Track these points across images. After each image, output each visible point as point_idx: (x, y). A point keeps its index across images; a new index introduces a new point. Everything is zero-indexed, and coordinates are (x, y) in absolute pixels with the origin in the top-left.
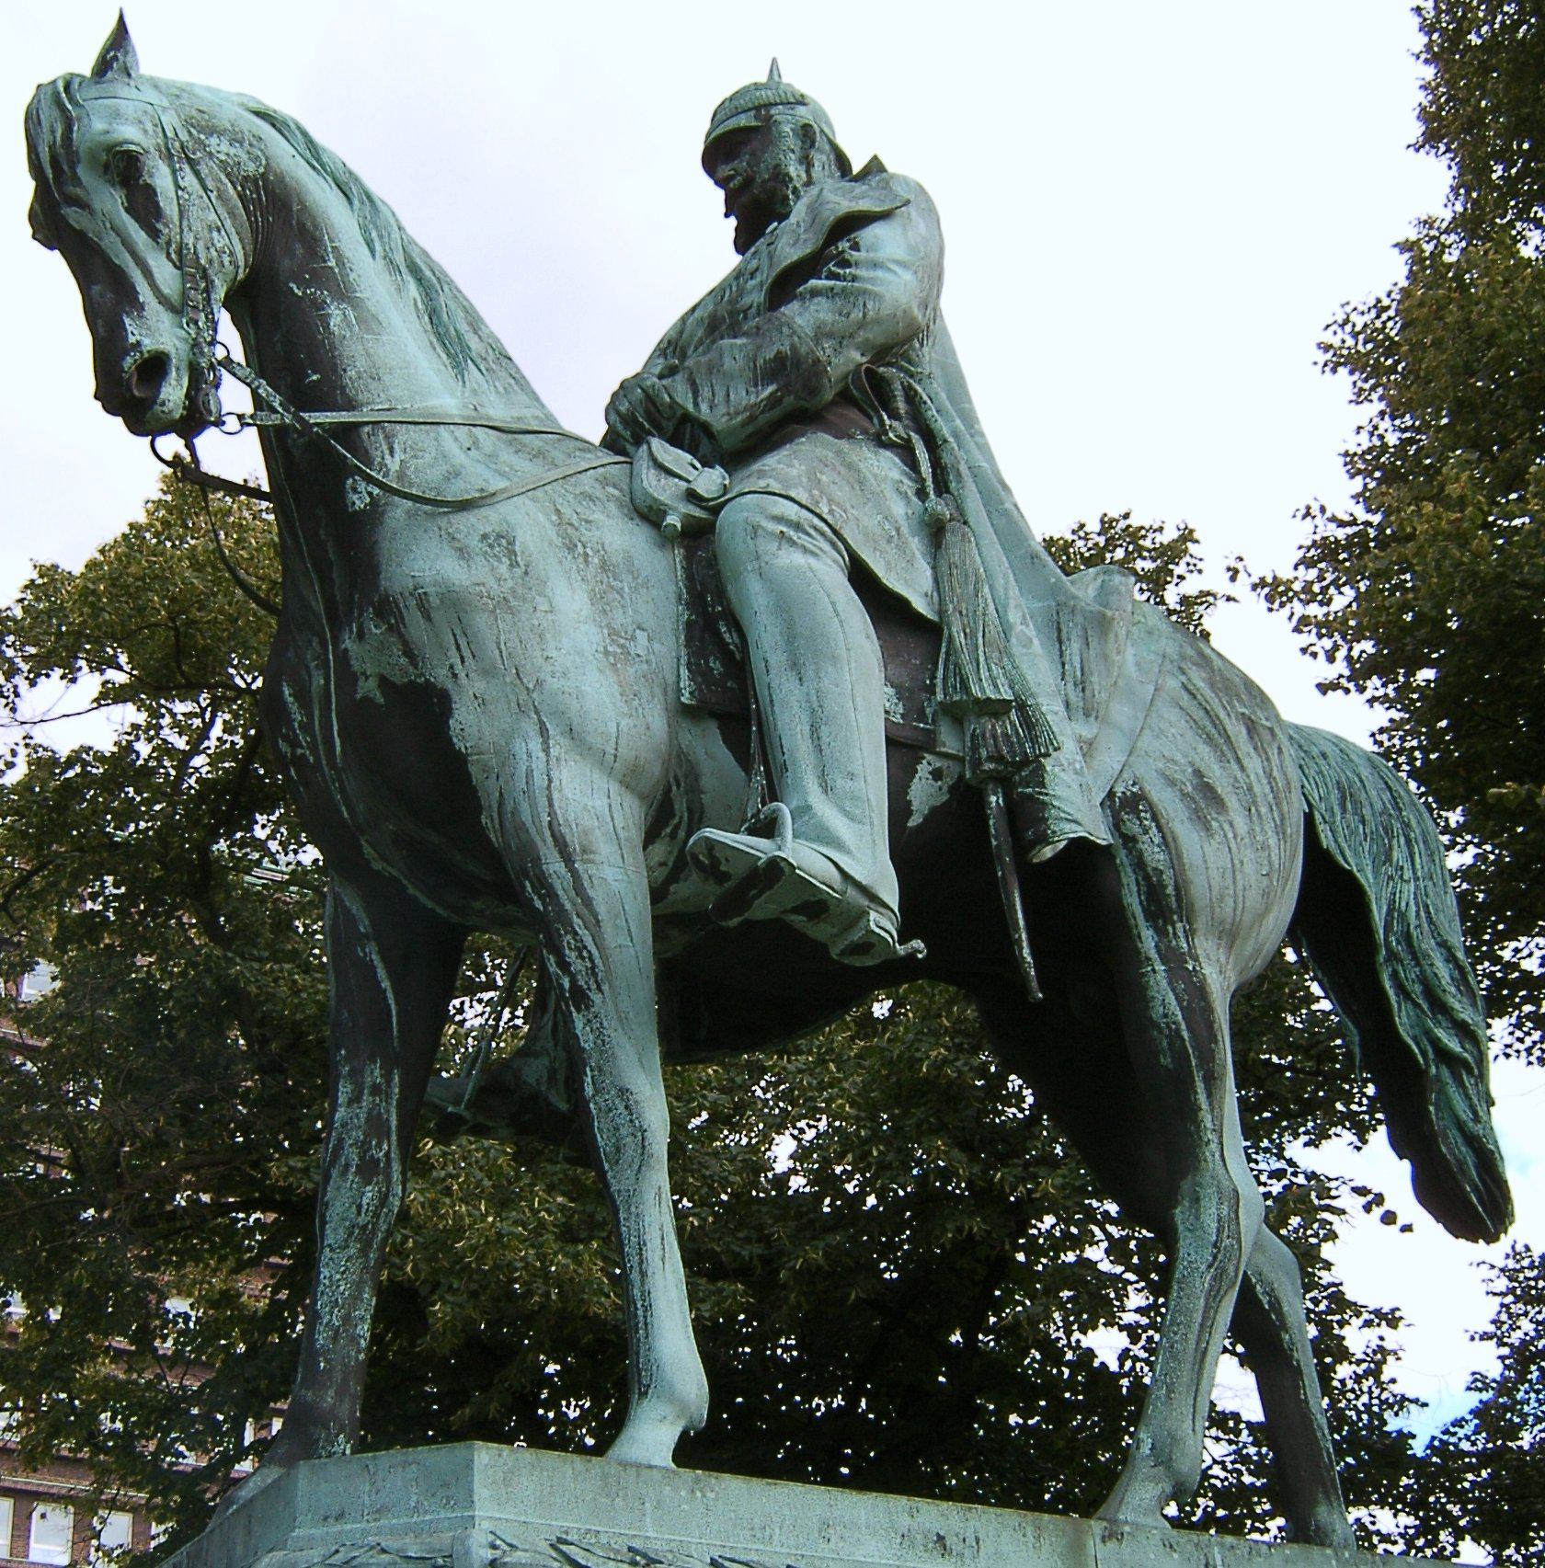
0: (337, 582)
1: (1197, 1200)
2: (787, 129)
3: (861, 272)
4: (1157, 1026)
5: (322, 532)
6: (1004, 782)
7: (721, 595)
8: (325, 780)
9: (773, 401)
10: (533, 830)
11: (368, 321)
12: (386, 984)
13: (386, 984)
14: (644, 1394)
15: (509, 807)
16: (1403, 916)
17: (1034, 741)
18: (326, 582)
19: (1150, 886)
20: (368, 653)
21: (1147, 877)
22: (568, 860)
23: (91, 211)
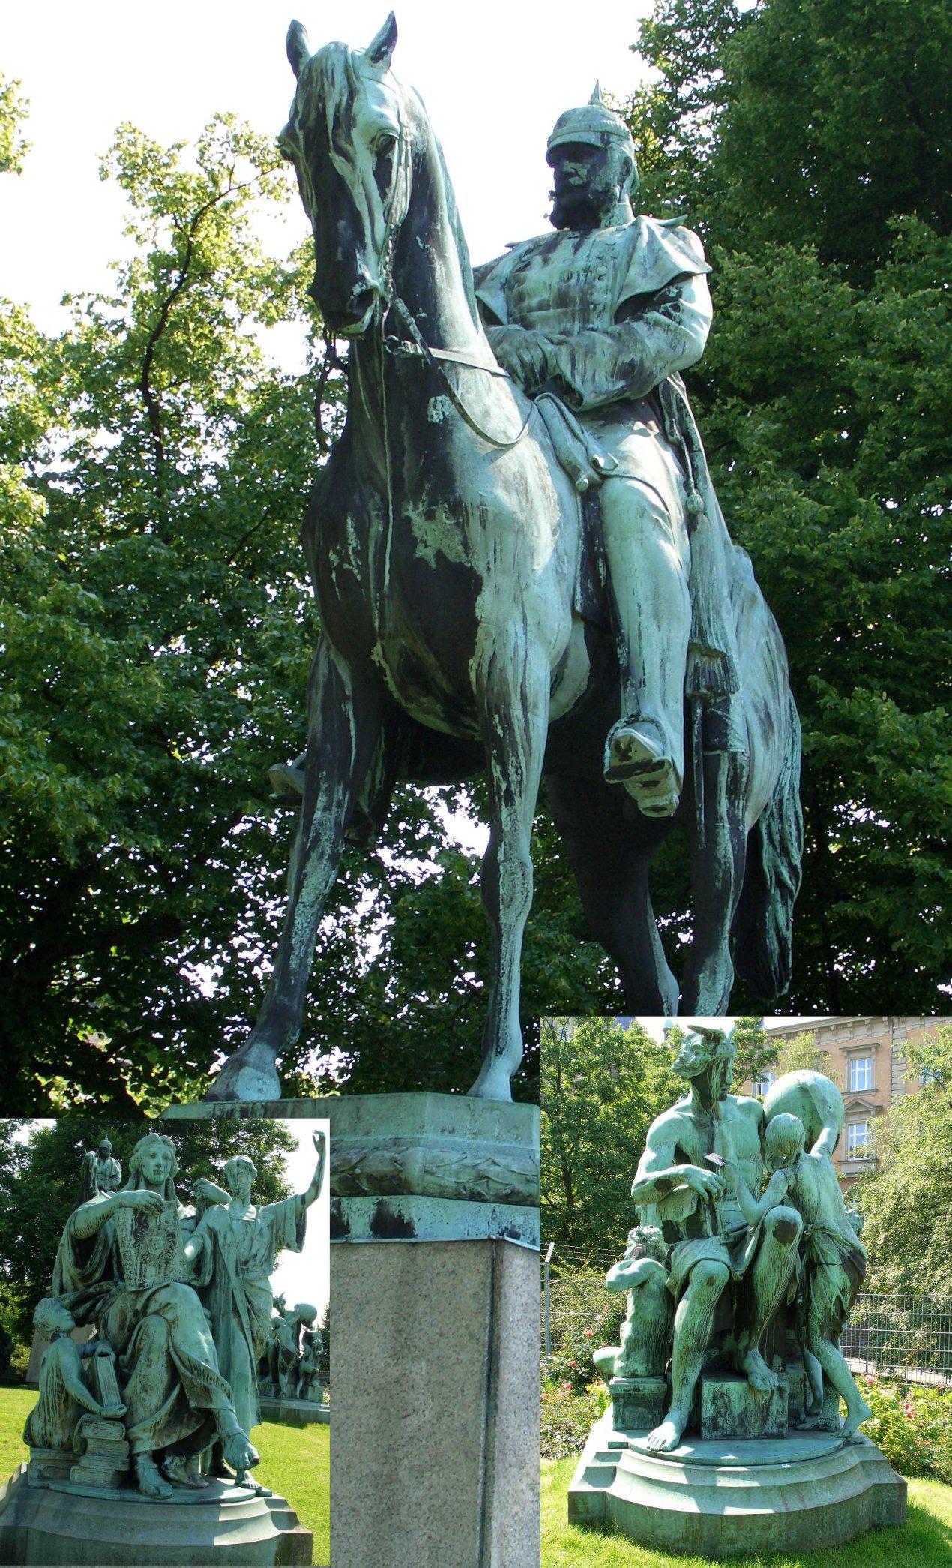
0: (407, 465)
1: (715, 973)
2: (617, 155)
3: (685, 318)
4: (718, 861)
5: (403, 425)
7: (603, 544)
8: (368, 596)
9: (622, 391)
10: (511, 686)
11: (448, 274)
12: (353, 733)
13: (353, 733)
14: (499, 1053)
15: (499, 665)
16: (782, 789)
17: (728, 680)
19: (735, 773)
20: (433, 536)
21: (735, 768)
23: (354, 166)
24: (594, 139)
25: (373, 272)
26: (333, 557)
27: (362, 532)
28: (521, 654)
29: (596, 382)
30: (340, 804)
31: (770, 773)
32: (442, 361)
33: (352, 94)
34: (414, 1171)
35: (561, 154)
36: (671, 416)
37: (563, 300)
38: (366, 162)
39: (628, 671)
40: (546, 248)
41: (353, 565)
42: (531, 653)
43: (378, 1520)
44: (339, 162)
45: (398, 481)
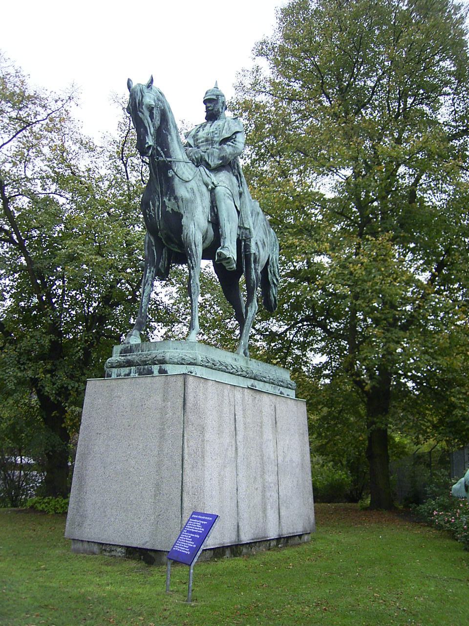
6: (245, 241)
7: (216, 203)
11: (172, 139)
18: (161, 188)
20: (170, 205)
22: (195, 247)
24: (214, 97)
25: (150, 141)
26: (147, 211)
27: (154, 205)
28: (194, 233)
29: (214, 162)
30: (153, 272)
31: (265, 256)
32: (170, 162)
33: (142, 97)
34: (167, 358)
35: (205, 102)
36: (235, 168)
37: (207, 140)
38: (147, 114)
39: (222, 235)
40: (203, 126)
41: (152, 213)
42: (196, 232)
43: (161, 438)
44: (140, 114)
45: (161, 191)
